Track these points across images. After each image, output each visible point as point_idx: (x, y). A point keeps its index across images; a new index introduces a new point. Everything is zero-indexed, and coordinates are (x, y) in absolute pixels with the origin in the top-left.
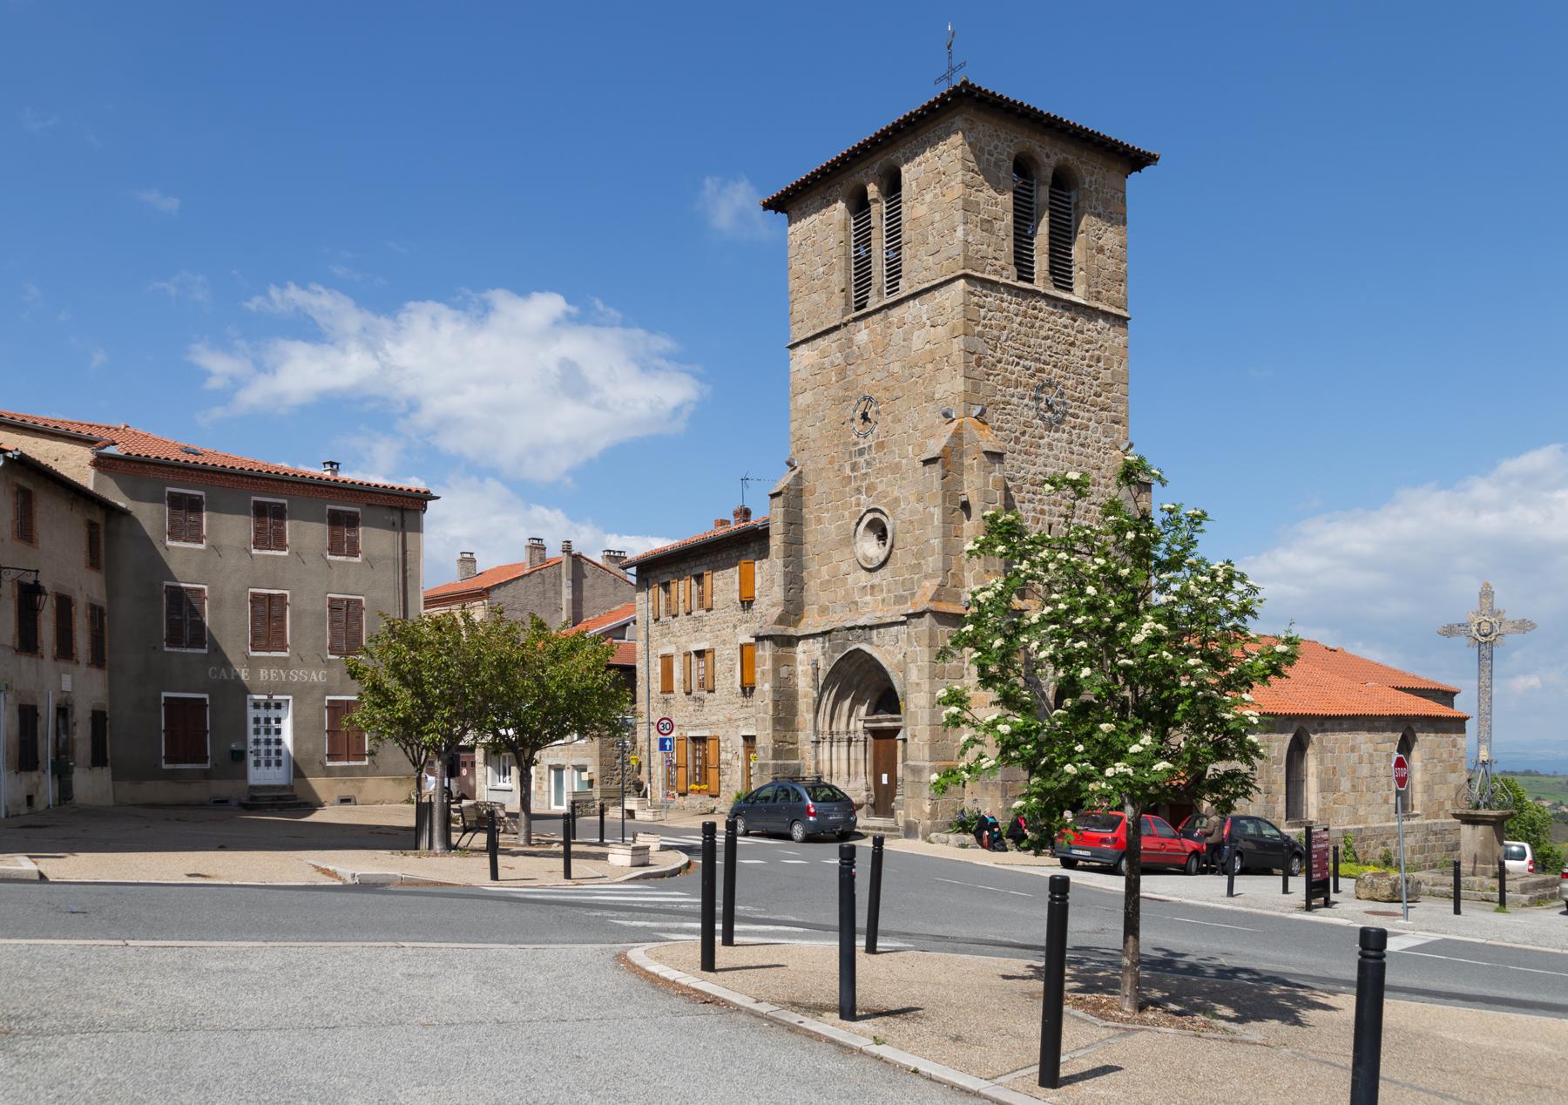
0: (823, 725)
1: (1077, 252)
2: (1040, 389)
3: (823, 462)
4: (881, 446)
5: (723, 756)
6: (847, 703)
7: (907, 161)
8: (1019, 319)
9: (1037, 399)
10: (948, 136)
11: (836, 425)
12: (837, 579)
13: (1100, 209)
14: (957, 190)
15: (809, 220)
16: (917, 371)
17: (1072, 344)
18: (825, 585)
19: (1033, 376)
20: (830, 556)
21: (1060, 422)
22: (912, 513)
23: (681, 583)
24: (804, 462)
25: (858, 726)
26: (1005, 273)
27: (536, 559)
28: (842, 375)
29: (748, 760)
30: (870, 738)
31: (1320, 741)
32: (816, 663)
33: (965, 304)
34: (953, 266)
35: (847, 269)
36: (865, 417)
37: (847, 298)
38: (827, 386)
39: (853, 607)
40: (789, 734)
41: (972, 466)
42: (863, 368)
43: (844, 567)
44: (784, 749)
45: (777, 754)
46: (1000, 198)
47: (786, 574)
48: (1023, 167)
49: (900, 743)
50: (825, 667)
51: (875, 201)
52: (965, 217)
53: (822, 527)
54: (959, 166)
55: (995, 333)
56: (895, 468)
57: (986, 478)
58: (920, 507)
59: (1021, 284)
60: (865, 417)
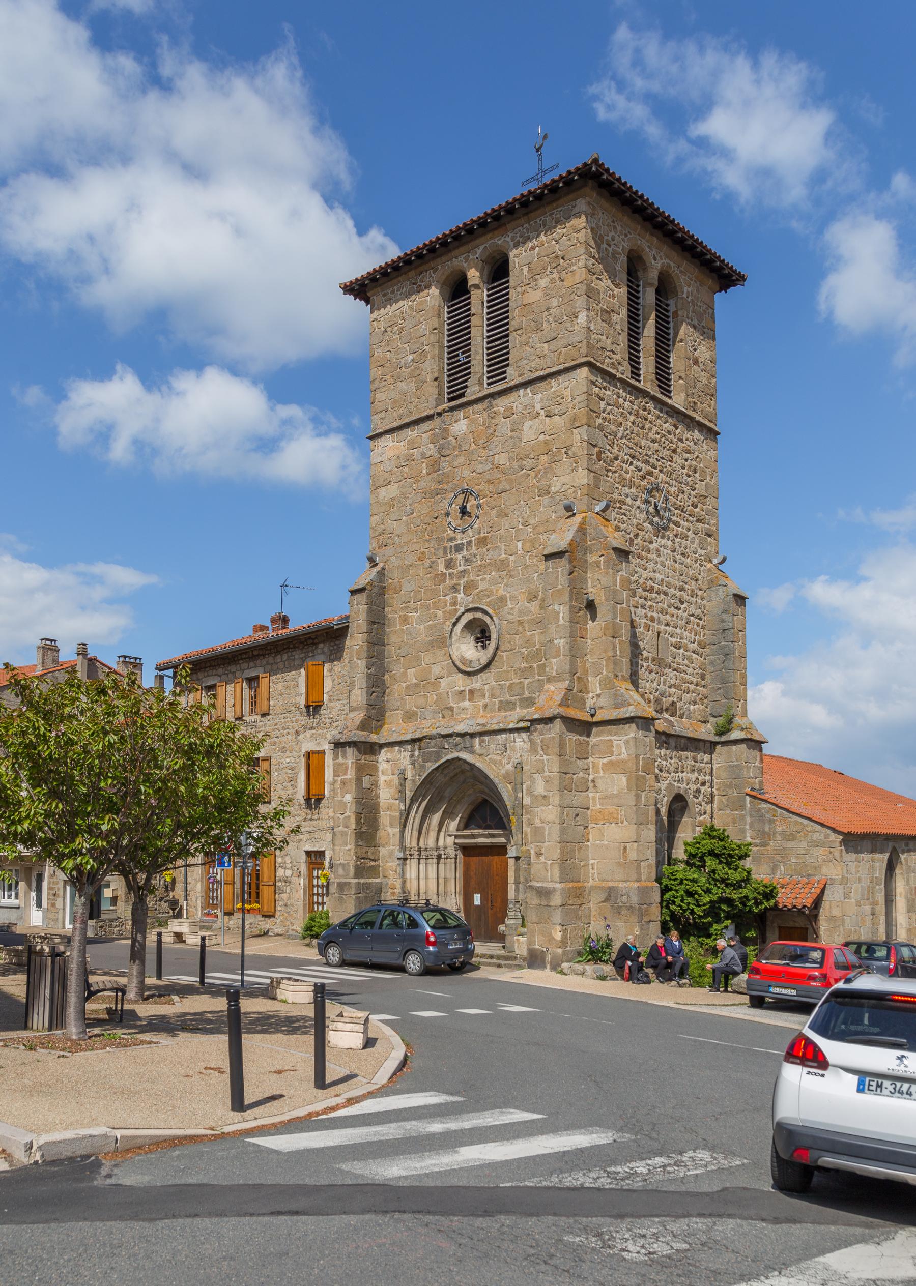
0: (410, 840)
1: (675, 359)
2: (650, 492)
3: (411, 559)
5: (280, 873)
6: (436, 818)
7: (516, 246)
8: (632, 418)
9: (647, 502)
10: (568, 218)
11: (427, 520)
13: (695, 322)
14: (580, 274)
15: (395, 306)
16: (528, 463)
17: (674, 451)
18: (412, 690)
19: (643, 478)
20: (418, 658)
21: (665, 528)
22: (521, 612)
23: (230, 688)
24: (390, 559)
25: (448, 842)
26: (620, 368)
27: (49, 661)
28: (435, 467)
29: (311, 877)
30: (460, 855)
31: (906, 860)
32: (403, 772)
33: (588, 393)
34: (574, 353)
36: (464, 511)
37: (440, 387)
38: (416, 478)
40: (371, 850)
41: (597, 564)
42: (461, 460)
43: (436, 670)
44: (366, 866)
46: (616, 291)
47: (369, 676)
48: (634, 267)
49: (511, 862)
51: (477, 287)
53: (409, 627)
54: (582, 250)
55: (613, 428)
58: (534, 607)
59: (632, 381)
60: (464, 511)
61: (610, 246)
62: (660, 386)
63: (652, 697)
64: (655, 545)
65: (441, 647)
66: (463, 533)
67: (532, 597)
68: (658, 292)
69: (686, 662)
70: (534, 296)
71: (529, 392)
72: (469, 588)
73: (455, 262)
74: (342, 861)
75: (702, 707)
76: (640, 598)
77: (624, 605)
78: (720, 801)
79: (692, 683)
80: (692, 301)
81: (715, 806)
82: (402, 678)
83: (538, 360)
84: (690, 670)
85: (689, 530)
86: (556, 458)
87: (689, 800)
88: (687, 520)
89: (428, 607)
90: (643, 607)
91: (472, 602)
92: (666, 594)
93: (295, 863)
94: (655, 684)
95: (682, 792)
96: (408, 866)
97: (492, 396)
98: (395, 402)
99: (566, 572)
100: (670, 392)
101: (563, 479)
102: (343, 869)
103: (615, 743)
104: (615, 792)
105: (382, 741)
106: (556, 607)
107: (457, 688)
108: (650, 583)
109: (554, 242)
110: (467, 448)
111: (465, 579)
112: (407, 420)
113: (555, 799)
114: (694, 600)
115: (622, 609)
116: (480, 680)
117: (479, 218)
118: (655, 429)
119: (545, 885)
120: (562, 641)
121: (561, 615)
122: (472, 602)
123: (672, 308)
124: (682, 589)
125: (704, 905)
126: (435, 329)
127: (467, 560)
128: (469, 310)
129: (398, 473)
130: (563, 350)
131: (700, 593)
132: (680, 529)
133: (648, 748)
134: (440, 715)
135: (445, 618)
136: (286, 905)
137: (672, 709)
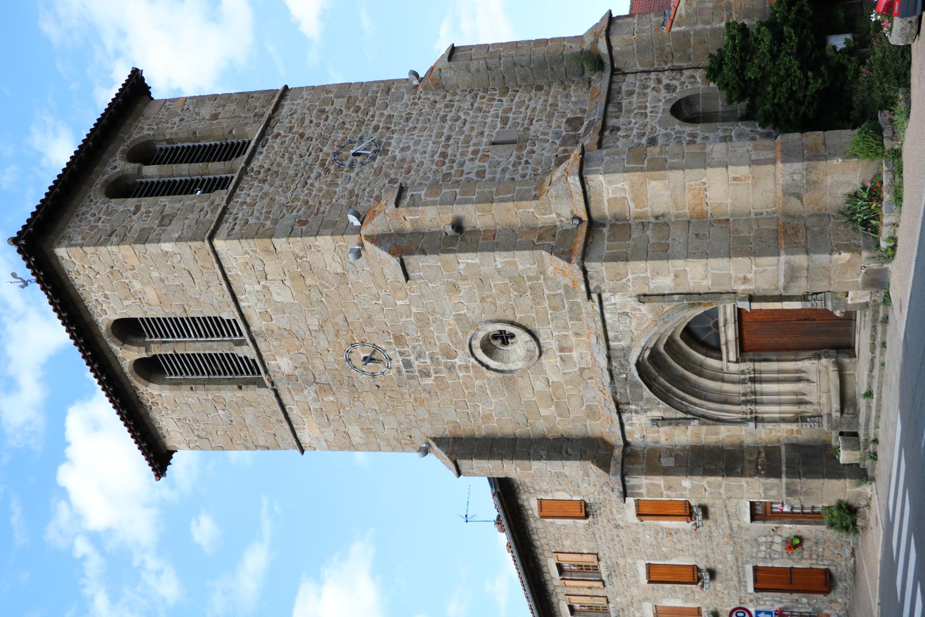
0: (735, 412)
3: (422, 413)
4: (399, 340)
9: (352, 166)
11: (380, 395)
12: (554, 396)
18: (563, 411)
19: (327, 171)
28: (325, 388)
32: (655, 422)
33: (241, 237)
35: (218, 382)
39: (587, 374)
40: (747, 457)
42: (317, 362)
43: (540, 386)
45: (772, 471)
47: (549, 458)
49: (756, 306)
50: (661, 410)
52: (152, 241)
53: (495, 414)
56: (422, 322)
57: (426, 204)
58: (464, 286)
59: (231, 188)
61: (100, 218)
62: (237, 157)
63: (561, 149)
64: (397, 153)
65: (515, 381)
66: (391, 359)
67: (455, 288)
68: (147, 163)
69: (523, 110)
70: (151, 294)
71: (243, 297)
72: (449, 354)
73: (126, 370)
74: (761, 491)
75: (573, 87)
76: (452, 167)
77: (458, 190)
78: (680, 59)
79: (546, 101)
80: (157, 124)
81: (685, 65)
82: (548, 420)
83: (212, 289)
84: (532, 104)
85: (382, 115)
86: (308, 268)
87: (679, 98)
88: (373, 116)
89: (472, 395)
90: (462, 164)
91: (464, 350)
92: (449, 138)
93: (766, 533)
94: (547, 145)
95: (669, 107)
96: (765, 416)
97: (249, 332)
98: (265, 426)
99: (423, 257)
100: (244, 143)
101: (329, 260)
102: (771, 489)
103: (611, 196)
104: (669, 193)
105: (621, 443)
106: (461, 266)
107: (558, 364)
108: (436, 158)
109: (98, 276)
110: (304, 357)
111: (440, 357)
112: (282, 416)
113: (679, 264)
114: (456, 104)
115: (462, 193)
116: (548, 341)
117: (80, 350)
118: (278, 159)
119: (782, 273)
120: (497, 259)
121: (469, 261)
122: (464, 350)
123: (164, 145)
124: (444, 119)
125: (807, 77)
126: (192, 388)
127: (419, 356)
128: (171, 355)
129: (335, 424)
130: (200, 263)
131: (449, 98)
132: (381, 125)
133: (616, 157)
134: (590, 381)
135: (483, 377)
136: (817, 543)
137: (574, 123)
